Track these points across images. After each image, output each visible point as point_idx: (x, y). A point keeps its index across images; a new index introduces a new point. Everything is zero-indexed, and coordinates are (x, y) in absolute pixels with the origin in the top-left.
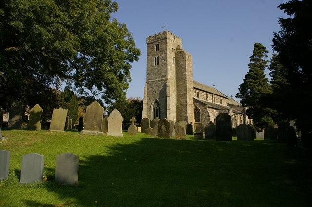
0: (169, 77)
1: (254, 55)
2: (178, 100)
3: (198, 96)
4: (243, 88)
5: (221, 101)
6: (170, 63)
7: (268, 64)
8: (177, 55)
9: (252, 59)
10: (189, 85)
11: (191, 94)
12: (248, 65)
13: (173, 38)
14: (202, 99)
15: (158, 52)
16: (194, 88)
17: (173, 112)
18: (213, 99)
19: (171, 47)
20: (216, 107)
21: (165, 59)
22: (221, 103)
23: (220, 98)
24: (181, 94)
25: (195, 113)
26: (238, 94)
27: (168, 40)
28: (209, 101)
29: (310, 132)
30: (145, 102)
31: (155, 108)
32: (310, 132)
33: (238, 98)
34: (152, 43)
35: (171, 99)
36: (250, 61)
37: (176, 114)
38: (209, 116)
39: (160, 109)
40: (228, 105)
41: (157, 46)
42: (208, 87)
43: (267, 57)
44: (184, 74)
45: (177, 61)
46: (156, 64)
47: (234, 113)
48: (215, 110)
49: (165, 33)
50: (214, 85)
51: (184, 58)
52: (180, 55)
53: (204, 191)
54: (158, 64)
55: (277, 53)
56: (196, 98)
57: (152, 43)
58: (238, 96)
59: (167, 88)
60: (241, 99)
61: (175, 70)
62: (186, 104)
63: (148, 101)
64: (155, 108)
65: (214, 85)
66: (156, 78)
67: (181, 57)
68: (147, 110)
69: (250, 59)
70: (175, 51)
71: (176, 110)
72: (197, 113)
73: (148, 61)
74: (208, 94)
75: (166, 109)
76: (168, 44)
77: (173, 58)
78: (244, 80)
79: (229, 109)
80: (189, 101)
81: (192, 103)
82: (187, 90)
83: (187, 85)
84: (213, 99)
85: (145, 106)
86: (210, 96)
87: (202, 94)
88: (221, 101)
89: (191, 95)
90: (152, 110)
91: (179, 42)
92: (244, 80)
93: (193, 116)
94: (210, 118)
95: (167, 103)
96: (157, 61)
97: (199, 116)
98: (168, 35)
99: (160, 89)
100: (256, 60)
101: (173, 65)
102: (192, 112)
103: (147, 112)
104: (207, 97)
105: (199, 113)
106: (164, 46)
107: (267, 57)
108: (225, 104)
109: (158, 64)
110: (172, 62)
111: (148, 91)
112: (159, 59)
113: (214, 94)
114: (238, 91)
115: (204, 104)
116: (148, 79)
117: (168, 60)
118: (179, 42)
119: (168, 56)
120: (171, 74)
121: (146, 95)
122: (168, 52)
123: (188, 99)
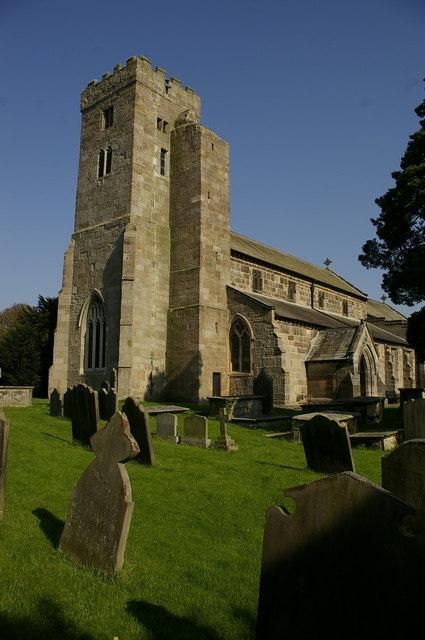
0: (137, 210)
2: (173, 294)
4: (394, 212)
6: (147, 165)
8: (175, 141)
11: (218, 275)
13: (161, 86)
14: (273, 290)
16: (234, 253)
17: (147, 334)
19: (153, 116)
20: (315, 321)
22: (345, 312)
25: (233, 339)
26: (369, 247)
27: (137, 86)
30: (65, 301)
31: (94, 321)
34: (93, 107)
37: (164, 343)
38: (278, 352)
41: (108, 113)
42: (306, 265)
47: (377, 340)
48: (308, 332)
50: (328, 262)
51: (195, 148)
52: (183, 140)
53: (404, 294)
54: (108, 171)
56: (248, 290)
57: (93, 107)
58: (370, 255)
59: (126, 248)
60: (387, 271)
61: (165, 189)
62: (132, 307)
63: (76, 296)
65: (328, 262)
66: (99, 219)
67: (186, 147)
68: (71, 330)
71: (163, 329)
72: (240, 342)
73: (82, 165)
74: (295, 280)
76: (139, 102)
77: (157, 149)
78: (395, 175)
81: (223, 305)
82: (204, 256)
83: (203, 238)
84: (317, 298)
85: (63, 317)
86: (303, 288)
90: (84, 330)
91: (191, 105)
92: (395, 175)
93: (227, 350)
95: (123, 302)
96: (106, 164)
97: (246, 354)
99: (108, 255)
101: (157, 174)
102: (224, 336)
103: (70, 335)
104: (292, 292)
105: (246, 337)
106: (128, 106)
110: (156, 161)
111: (75, 266)
112: (109, 156)
114: (372, 233)
115: (262, 309)
116: (79, 225)
118: (191, 105)
121: (70, 281)
122: (138, 126)
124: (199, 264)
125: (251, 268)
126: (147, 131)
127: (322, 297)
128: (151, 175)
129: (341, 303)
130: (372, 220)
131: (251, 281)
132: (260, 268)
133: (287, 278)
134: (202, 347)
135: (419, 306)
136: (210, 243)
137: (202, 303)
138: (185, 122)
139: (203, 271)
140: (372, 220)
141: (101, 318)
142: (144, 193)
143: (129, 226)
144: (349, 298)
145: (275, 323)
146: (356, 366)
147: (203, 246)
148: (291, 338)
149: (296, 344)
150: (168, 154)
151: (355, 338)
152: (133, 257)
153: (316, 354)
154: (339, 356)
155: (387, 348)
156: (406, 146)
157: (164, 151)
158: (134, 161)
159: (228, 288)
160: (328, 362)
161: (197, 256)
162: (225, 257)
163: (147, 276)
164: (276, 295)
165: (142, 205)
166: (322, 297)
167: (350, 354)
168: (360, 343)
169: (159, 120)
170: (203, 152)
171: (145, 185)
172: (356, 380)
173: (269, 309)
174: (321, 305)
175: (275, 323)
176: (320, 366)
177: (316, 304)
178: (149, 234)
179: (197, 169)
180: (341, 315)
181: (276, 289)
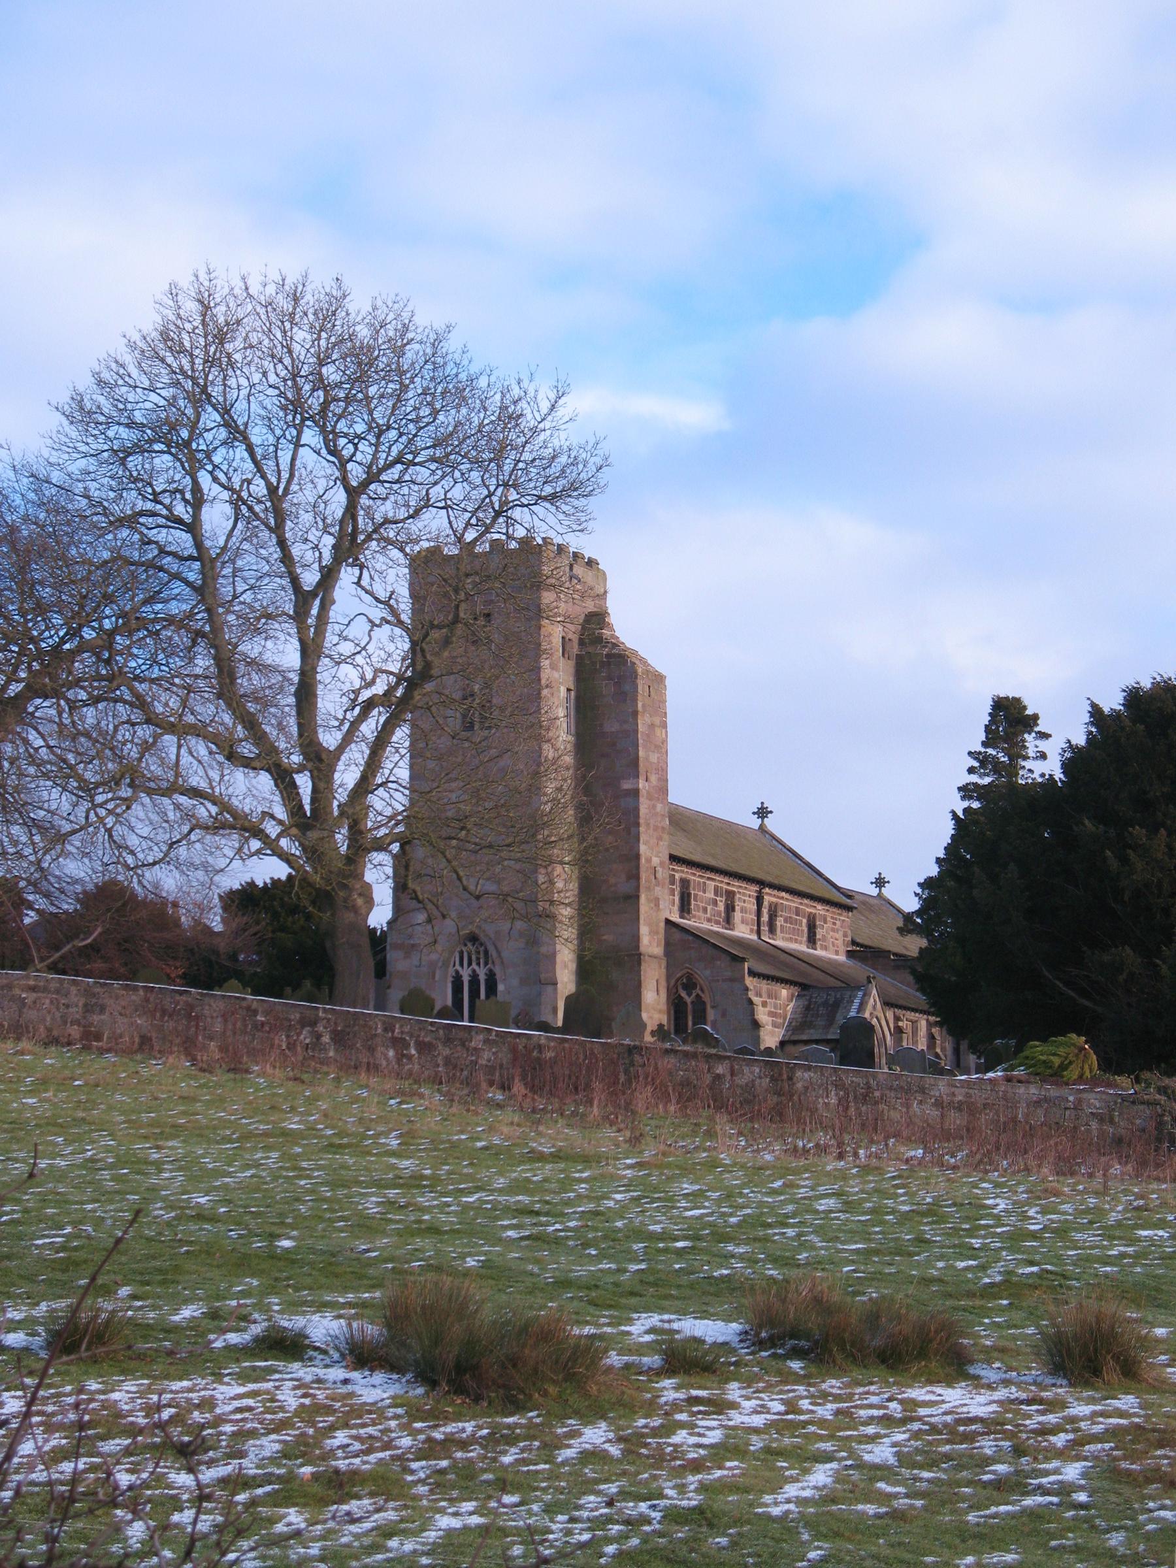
3: (685, 907)
5: (812, 927)
9: (983, 761)
11: (657, 901)
12: (960, 789)
16: (673, 858)
18: (765, 918)
22: (812, 940)
23: (808, 907)
33: (910, 932)
36: (984, 744)
38: (756, 1025)
43: (1043, 756)
44: (626, 785)
45: (586, 706)
47: (887, 1004)
49: (754, 813)
50: (763, 812)
55: (1058, 775)
56: (675, 918)
65: (763, 812)
69: (962, 793)
78: (938, 860)
80: (651, 942)
82: (643, 876)
83: (643, 848)
84: (765, 918)
86: (746, 896)
87: (707, 889)
88: (812, 927)
89: (656, 909)
92: (938, 860)
94: (762, 1033)
104: (730, 908)
108: (832, 950)
115: (732, 955)
123: (644, 930)
124: (638, 887)
125: (677, 876)
129: (805, 921)
133: (723, 883)
136: (649, 854)
137: (642, 949)
139: (643, 899)
144: (820, 909)
145: (749, 981)
147: (643, 861)
148: (764, 1004)
149: (771, 1014)
150: (573, 693)
155: (897, 1019)
156: (946, 831)
164: (709, 920)
172: (205, 1458)
175: (749, 981)
177: (765, 928)
181: (709, 908)
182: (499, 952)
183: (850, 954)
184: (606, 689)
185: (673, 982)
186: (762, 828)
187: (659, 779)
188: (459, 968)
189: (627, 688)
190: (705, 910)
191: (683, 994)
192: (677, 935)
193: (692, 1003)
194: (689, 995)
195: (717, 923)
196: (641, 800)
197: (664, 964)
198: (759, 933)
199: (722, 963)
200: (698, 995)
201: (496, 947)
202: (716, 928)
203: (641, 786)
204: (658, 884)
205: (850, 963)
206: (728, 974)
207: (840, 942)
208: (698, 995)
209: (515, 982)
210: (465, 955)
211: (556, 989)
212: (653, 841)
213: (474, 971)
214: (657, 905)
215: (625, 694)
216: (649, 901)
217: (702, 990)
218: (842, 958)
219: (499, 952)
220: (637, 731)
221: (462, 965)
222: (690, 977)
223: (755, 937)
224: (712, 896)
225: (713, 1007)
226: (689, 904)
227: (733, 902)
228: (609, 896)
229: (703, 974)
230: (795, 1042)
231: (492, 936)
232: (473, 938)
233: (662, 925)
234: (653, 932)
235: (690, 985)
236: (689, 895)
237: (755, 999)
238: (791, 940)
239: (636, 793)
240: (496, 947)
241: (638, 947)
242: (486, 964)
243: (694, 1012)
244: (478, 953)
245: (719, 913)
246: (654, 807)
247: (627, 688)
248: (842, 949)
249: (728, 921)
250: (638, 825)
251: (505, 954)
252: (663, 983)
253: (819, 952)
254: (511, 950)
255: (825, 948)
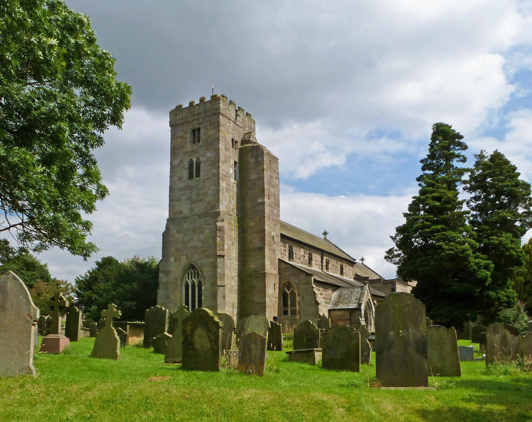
0: (222, 208)
1: (432, 156)
3: (291, 257)
5: (342, 268)
7: (466, 177)
10: (272, 231)
11: (274, 251)
12: (418, 179)
14: (300, 260)
15: (195, 147)
16: (283, 236)
21: (216, 162)
22: (342, 273)
24: (250, 249)
26: (390, 251)
28: (315, 268)
29: (318, 356)
31: (190, 282)
32: (318, 356)
35: (227, 262)
36: (423, 169)
38: (317, 303)
39: (200, 283)
40: (357, 277)
41: (196, 132)
42: (312, 237)
44: (260, 201)
45: (242, 168)
46: (191, 177)
50: (325, 233)
56: (287, 260)
64: (190, 282)
65: (325, 233)
70: (239, 146)
71: (236, 288)
75: (214, 285)
76: (222, 128)
78: (405, 215)
79: (362, 287)
80: (271, 268)
82: (267, 239)
83: (266, 227)
84: (324, 264)
86: (317, 257)
87: (299, 252)
88: (342, 268)
89: (274, 253)
92: (405, 215)
96: (194, 170)
98: (222, 106)
100: (437, 169)
104: (310, 259)
107: (464, 160)
109: (198, 175)
110: (231, 171)
113: (327, 252)
114: (393, 245)
117: (223, 167)
119: (222, 158)
120: (228, 203)
122: (222, 146)
123: (267, 262)
126: (227, 149)
127: (327, 263)
128: (229, 181)
130: (391, 237)
131: (287, 253)
132: (292, 243)
134: (267, 300)
135: (414, 283)
136: (270, 230)
138: (249, 142)
140: (391, 237)
141: (196, 281)
142: (227, 195)
143: (219, 218)
146: (363, 312)
147: (267, 232)
148: (321, 294)
149: (324, 298)
150: (238, 164)
151: (362, 294)
152: (223, 240)
153: (336, 304)
154: (353, 306)
157: (235, 162)
158: (220, 172)
159: (279, 260)
160: (344, 309)
161: (263, 239)
162: (278, 239)
163: (229, 252)
164: (301, 263)
165: (225, 203)
166: (327, 263)
167: (360, 305)
168: (365, 298)
169: (233, 140)
170: (265, 167)
171: (227, 188)
173: (311, 275)
174: (327, 268)
176: (339, 313)
177: (324, 268)
178: (230, 223)
179: (261, 179)
180: (339, 276)
182: (202, 273)
183: (355, 279)
184: (251, 160)
185: (282, 285)
186: (325, 238)
187: (275, 200)
188: (187, 280)
189: (260, 159)
190: (300, 259)
191: (287, 291)
192: (283, 266)
193: (290, 294)
194: (289, 290)
195: (305, 264)
196: (266, 206)
197: (278, 277)
198: (322, 269)
199: (302, 277)
200: (292, 291)
201: (201, 270)
202: (304, 266)
203: (265, 200)
204: (275, 243)
205: (355, 281)
206: (305, 281)
207: (351, 274)
208: (292, 291)
209: (209, 285)
210: (190, 274)
211: (225, 288)
212: (272, 225)
213: (193, 281)
214: (274, 252)
215: (258, 162)
216: (270, 250)
217: (294, 288)
218: (352, 280)
219: (202, 273)
220: (264, 177)
221: (188, 279)
222: (289, 282)
223: (320, 271)
224: (303, 254)
225: (298, 295)
226: (293, 256)
227: (311, 257)
228: (250, 249)
229: (294, 281)
230: (335, 310)
231: (200, 266)
232: (193, 267)
233: (277, 261)
234: (272, 264)
235: (289, 286)
236: (293, 252)
237: (316, 292)
238: (334, 272)
239: (263, 203)
240: (201, 270)
241: (264, 270)
242: (198, 278)
243: (291, 297)
244: (195, 273)
245: (306, 261)
246: (273, 211)
247: (260, 159)
248: (353, 277)
249: (310, 263)
250: (264, 217)
251: (205, 273)
252: (277, 285)
253: (344, 278)
254: (206, 271)
255: (347, 276)
